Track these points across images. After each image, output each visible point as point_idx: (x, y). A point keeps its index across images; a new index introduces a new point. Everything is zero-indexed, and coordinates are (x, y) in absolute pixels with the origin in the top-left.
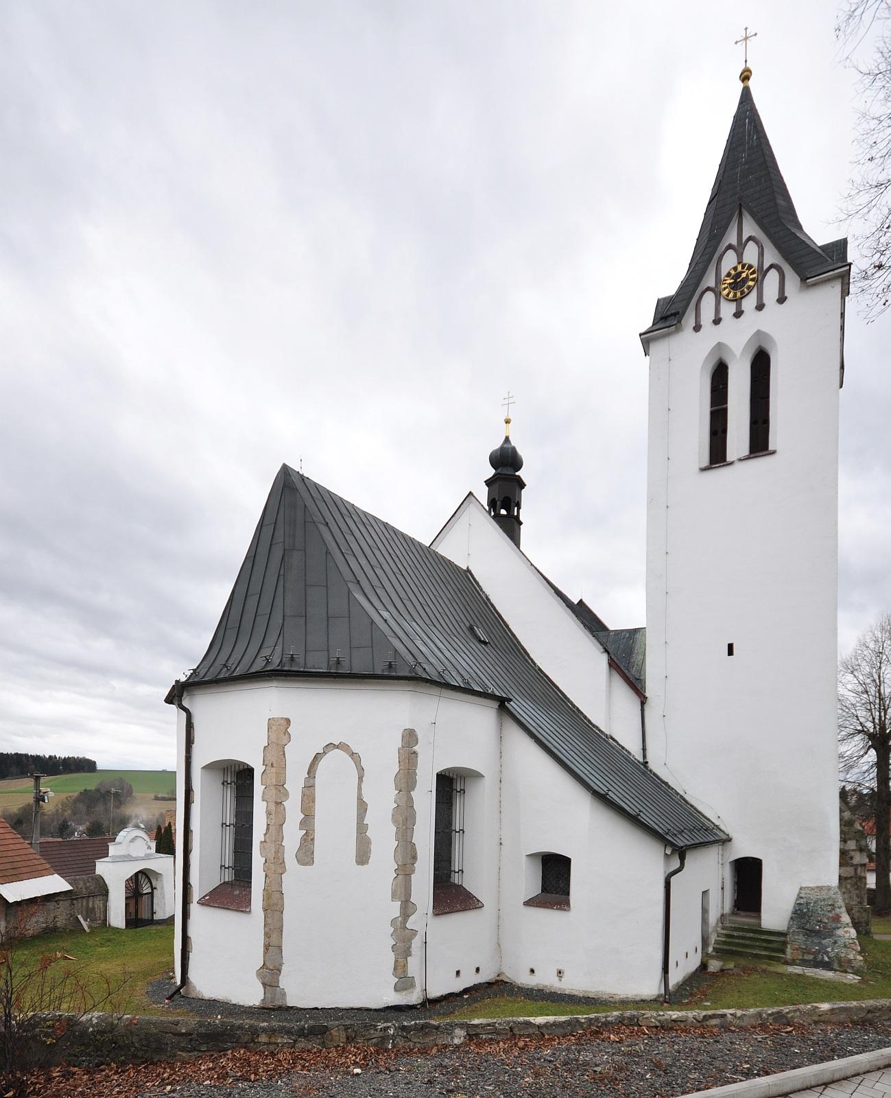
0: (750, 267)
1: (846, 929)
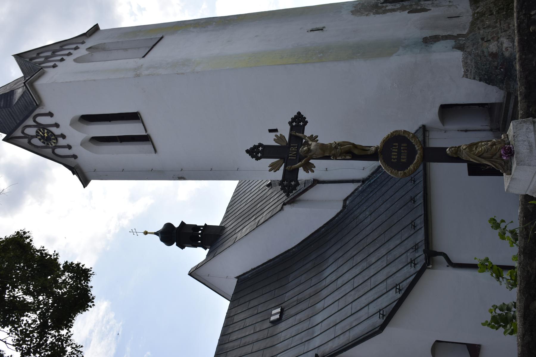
0: (37, 132)
1: (504, 49)
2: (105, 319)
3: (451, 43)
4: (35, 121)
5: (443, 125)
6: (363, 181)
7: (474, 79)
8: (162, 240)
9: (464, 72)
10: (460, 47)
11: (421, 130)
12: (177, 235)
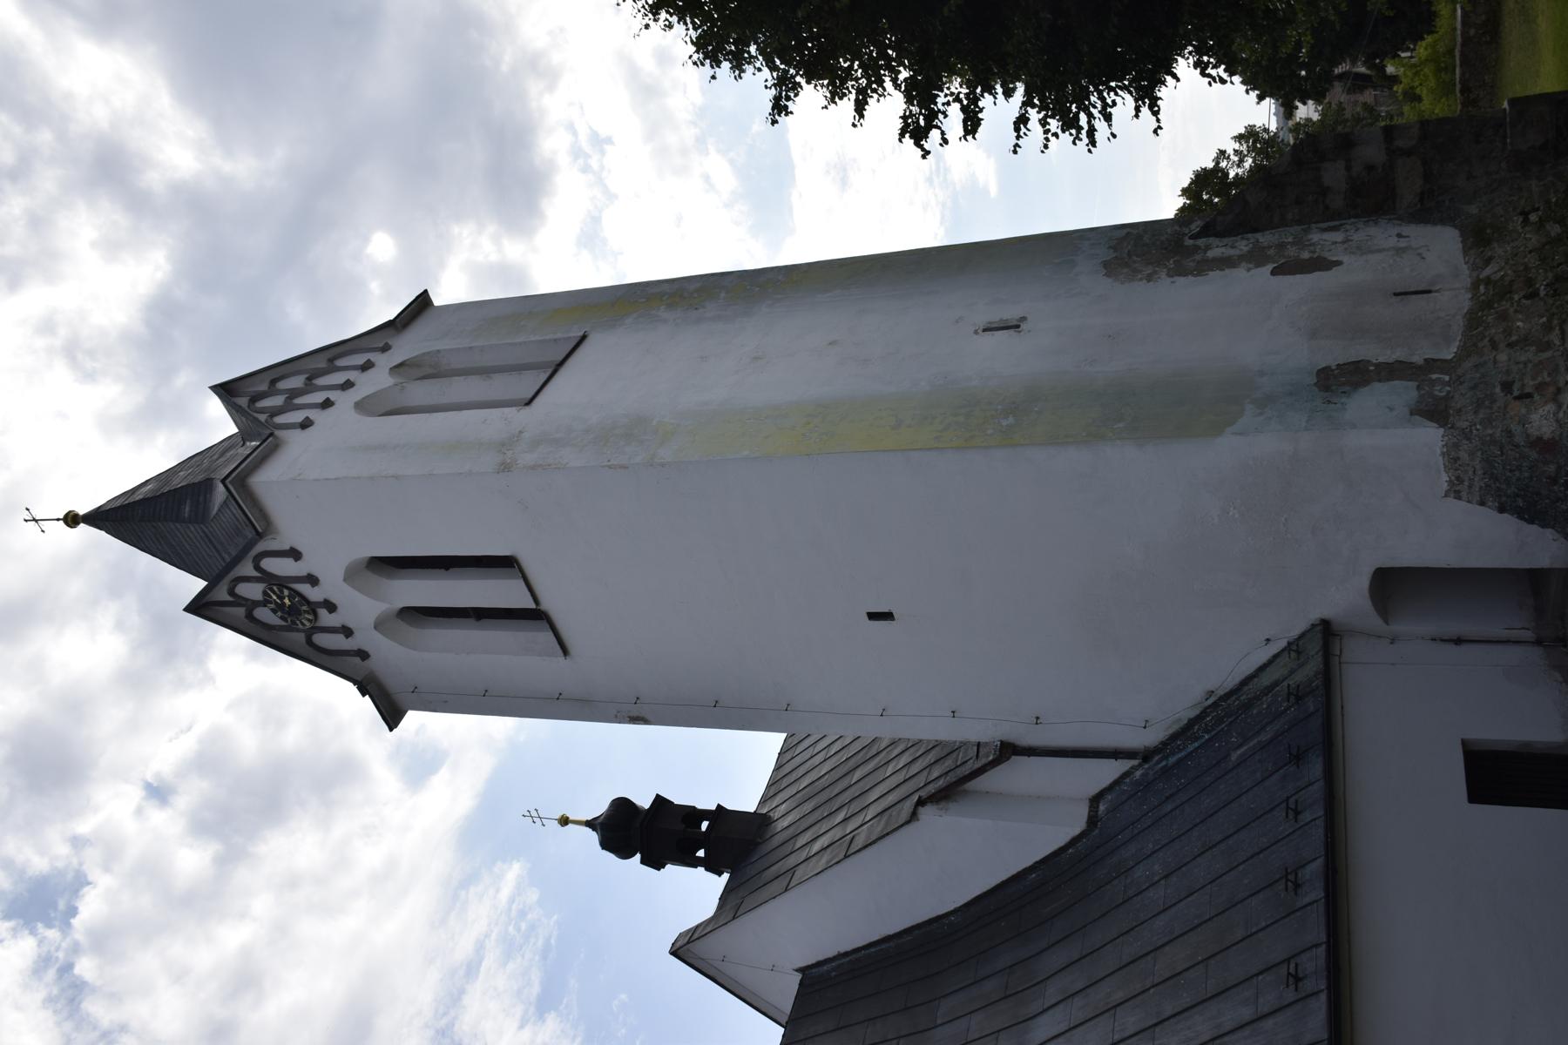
0: (265, 593)
2: (514, 906)
3: (1403, 393)
4: (257, 568)
5: (1387, 622)
6: (1146, 755)
7: (1482, 503)
8: (605, 845)
9: (1450, 482)
10: (1433, 411)
11: (1314, 647)
12: (645, 831)
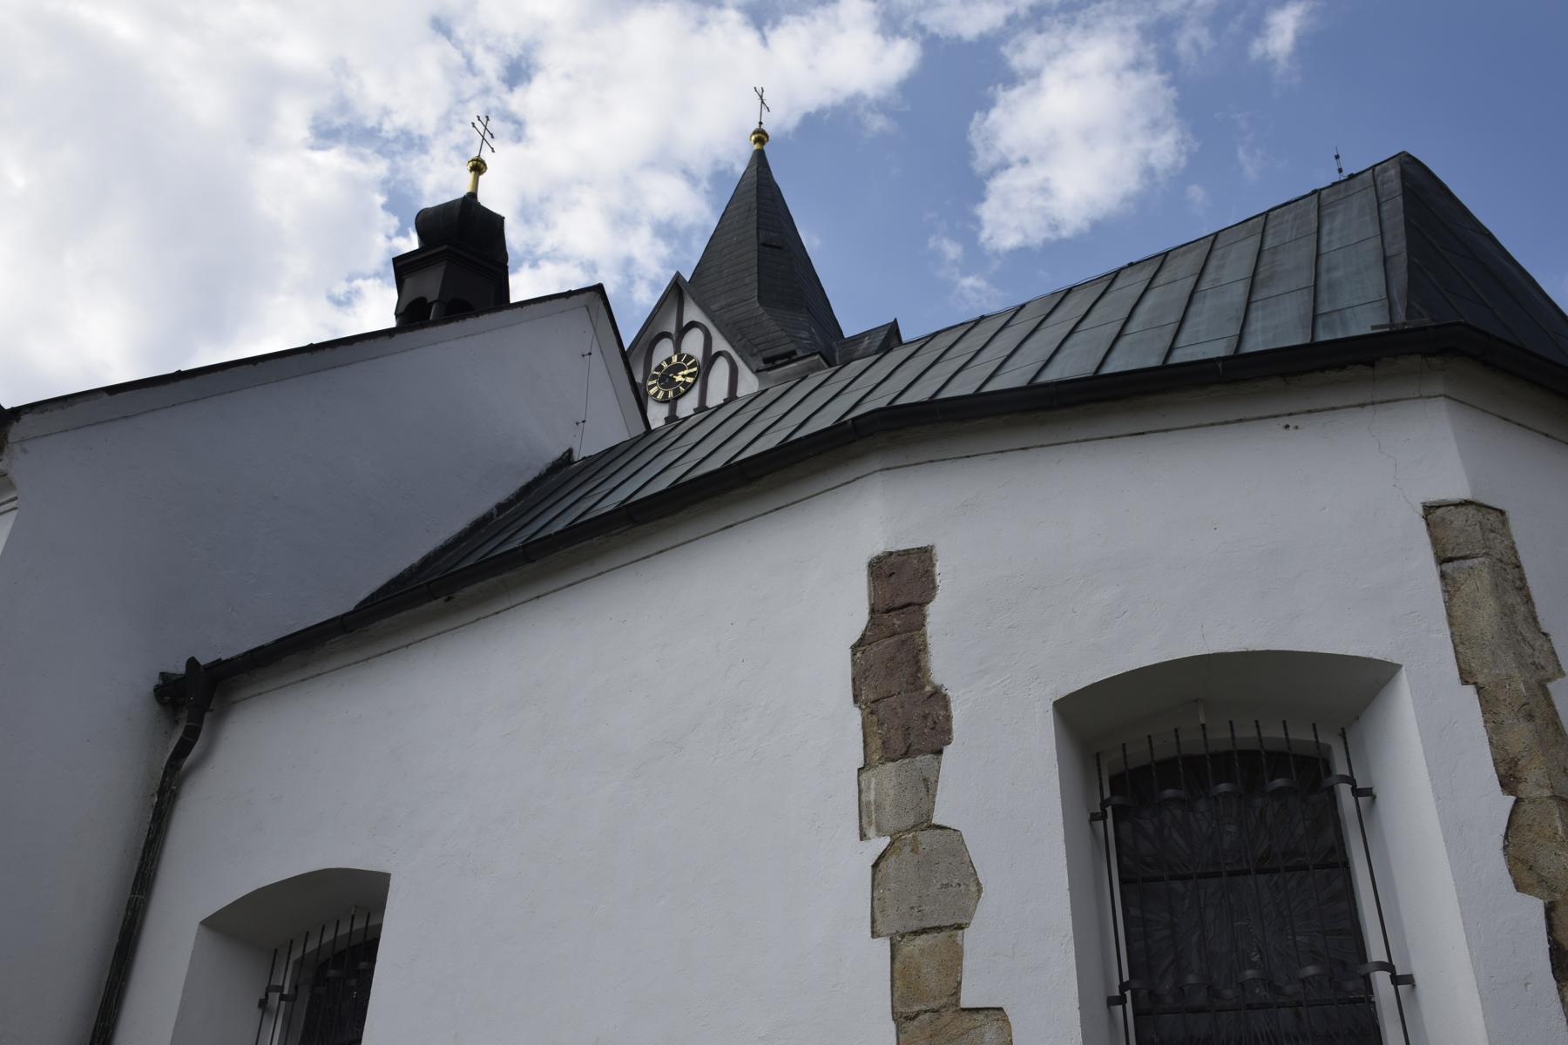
0: (689, 357)
